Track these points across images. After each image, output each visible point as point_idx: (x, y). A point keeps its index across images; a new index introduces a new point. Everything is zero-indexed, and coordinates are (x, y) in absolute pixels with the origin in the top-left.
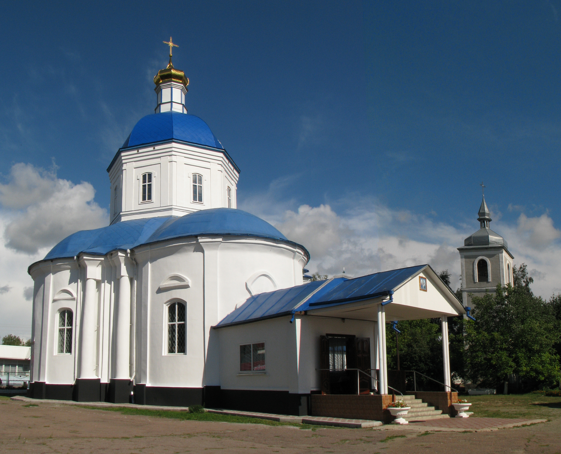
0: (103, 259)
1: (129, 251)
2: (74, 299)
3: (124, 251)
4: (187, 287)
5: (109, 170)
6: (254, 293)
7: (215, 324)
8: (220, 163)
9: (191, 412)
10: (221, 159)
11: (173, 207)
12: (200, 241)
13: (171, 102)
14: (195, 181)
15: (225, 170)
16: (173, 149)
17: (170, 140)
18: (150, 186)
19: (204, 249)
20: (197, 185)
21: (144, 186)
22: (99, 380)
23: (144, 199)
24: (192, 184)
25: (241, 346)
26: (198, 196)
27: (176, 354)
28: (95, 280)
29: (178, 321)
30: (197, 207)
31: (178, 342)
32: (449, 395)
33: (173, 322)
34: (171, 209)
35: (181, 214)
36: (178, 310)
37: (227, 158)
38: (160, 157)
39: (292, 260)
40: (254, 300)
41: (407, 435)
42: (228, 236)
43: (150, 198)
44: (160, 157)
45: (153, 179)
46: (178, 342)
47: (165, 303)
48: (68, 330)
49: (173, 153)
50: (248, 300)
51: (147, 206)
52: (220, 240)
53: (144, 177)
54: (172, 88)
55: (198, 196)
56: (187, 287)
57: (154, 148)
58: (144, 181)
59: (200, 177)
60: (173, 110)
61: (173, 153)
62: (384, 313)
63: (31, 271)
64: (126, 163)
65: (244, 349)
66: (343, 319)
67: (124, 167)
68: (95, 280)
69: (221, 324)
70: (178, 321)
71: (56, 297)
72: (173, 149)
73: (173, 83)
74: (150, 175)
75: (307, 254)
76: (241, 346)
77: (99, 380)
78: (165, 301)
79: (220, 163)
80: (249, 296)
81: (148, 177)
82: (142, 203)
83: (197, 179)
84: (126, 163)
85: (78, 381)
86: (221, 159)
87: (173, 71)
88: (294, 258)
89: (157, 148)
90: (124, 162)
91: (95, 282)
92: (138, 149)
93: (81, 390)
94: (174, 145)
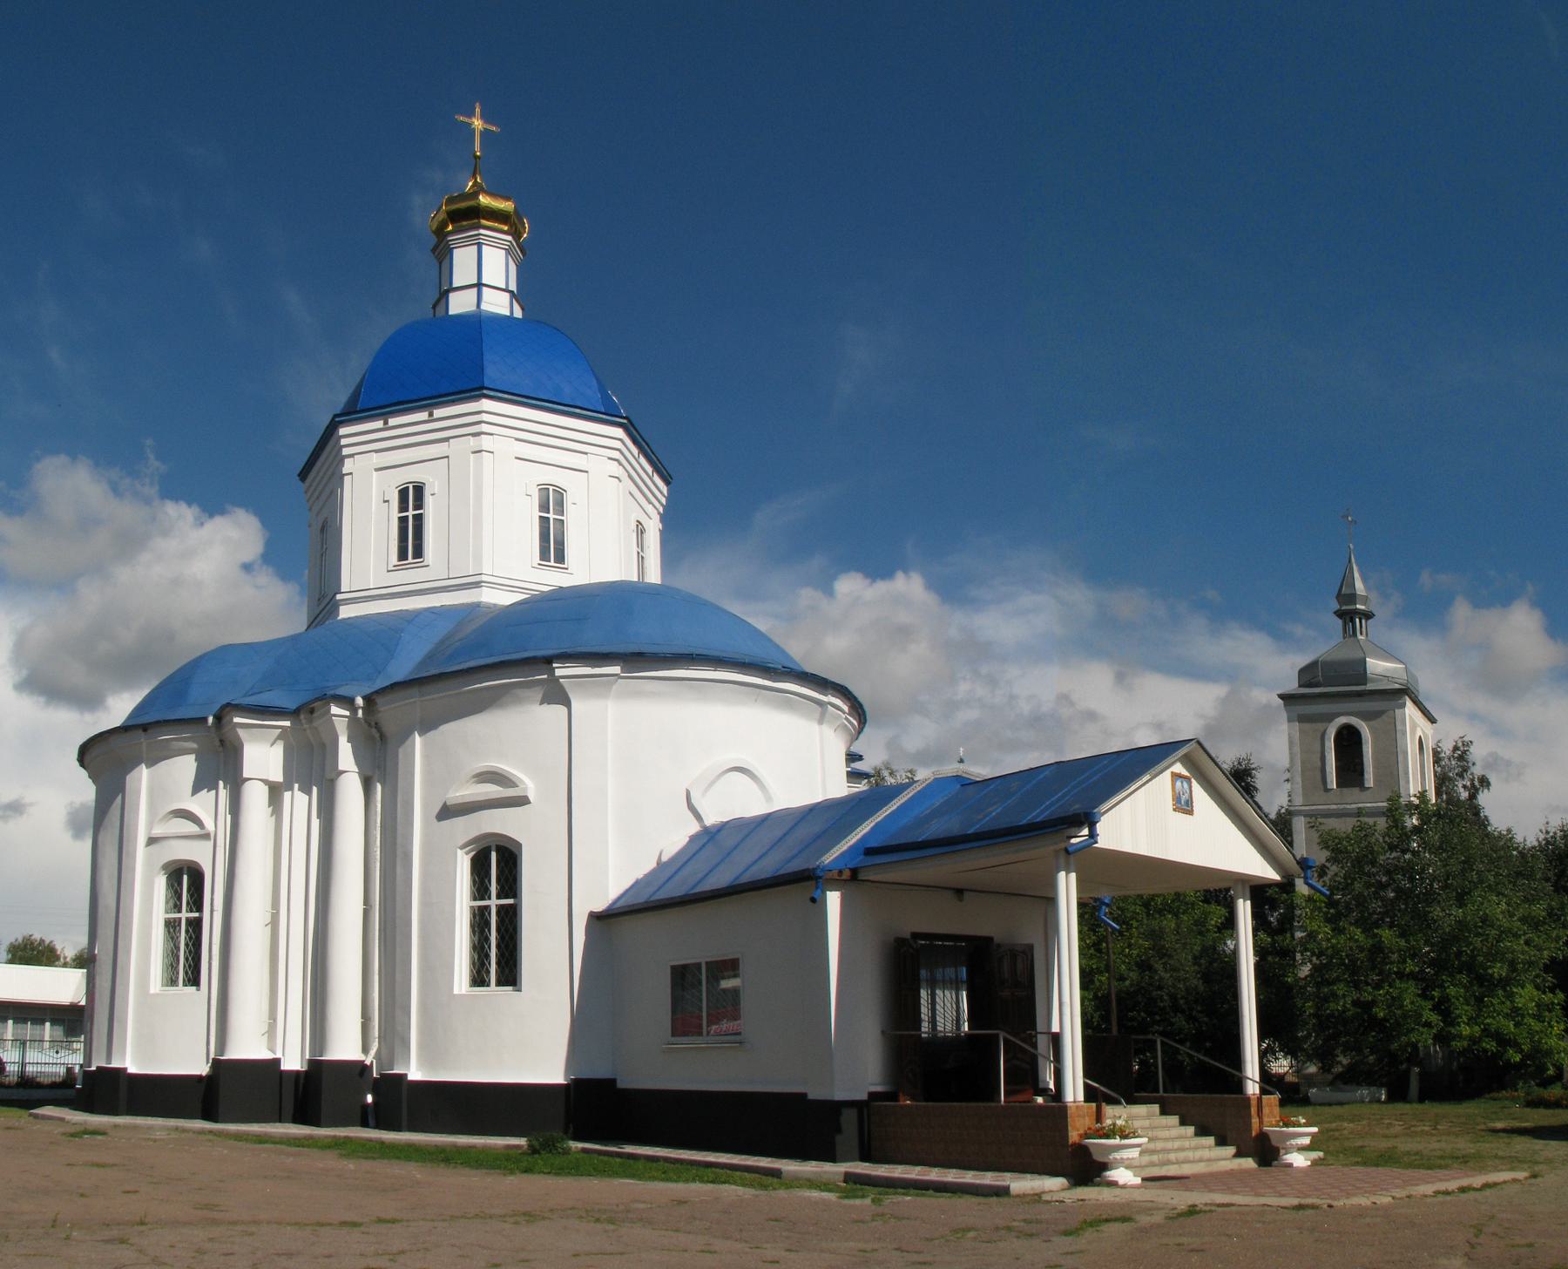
0: (288, 723)
1: (359, 701)
2: (206, 836)
3: (348, 702)
4: (522, 801)
5: (303, 475)
6: (711, 819)
7: (600, 906)
8: (616, 455)
9: (533, 1150)
10: (618, 444)
11: (484, 578)
12: (558, 672)
13: (479, 285)
14: (544, 507)
16: (485, 417)
17: (474, 390)
18: (419, 519)
20: (551, 516)
21: (403, 521)
22: (277, 1062)
23: (402, 555)
24: (537, 514)
25: (673, 968)
26: (552, 547)
27: (493, 991)
28: (265, 782)
29: (498, 897)
30: (551, 579)
31: (499, 956)
32: (1254, 1103)
33: (482, 899)
34: (477, 585)
35: (505, 599)
36: (498, 866)
38: (447, 440)
39: (815, 727)
40: (709, 837)
42: (637, 659)
43: (419, 553)
44: (447, 440)
45: (429, 501)
46: (499, 956)
48: (190, 922)
49: (485, 428)
50: (693, 839)
51: (412, 576)
52: (616, 669)
53: (403, 493)
54: (479, 245)
55: (552, 547)
56: (522, 801)
57: (431, 414)
58: (403, 506)
59: (560, 494)
61: (485, 428)
63: (87, 759)
64: (352, 456)
65: (682, 977)
66: (959, 892)
67: (348, 466)
68: (265, 782)
69: (619, 905)
70: (498, 897)
71: (158, 831)
72: (485, 417)
74: (419, 489)
75: (858, 709)
76: (673, 968)
77: (277, 1062)
79: (616, 455)
80: (695, 828)
81: (412, 496)
82: (397, 569)
83: (551, 501)
84: (352, 456)
85: (217, 1064)
86: (618, 444)
87: (484, 200)
88: (821, 722)
89: (438, 413)
90: (345, 451)
91: (266, 788)
93: (226, 1091)
94: (486, 404)
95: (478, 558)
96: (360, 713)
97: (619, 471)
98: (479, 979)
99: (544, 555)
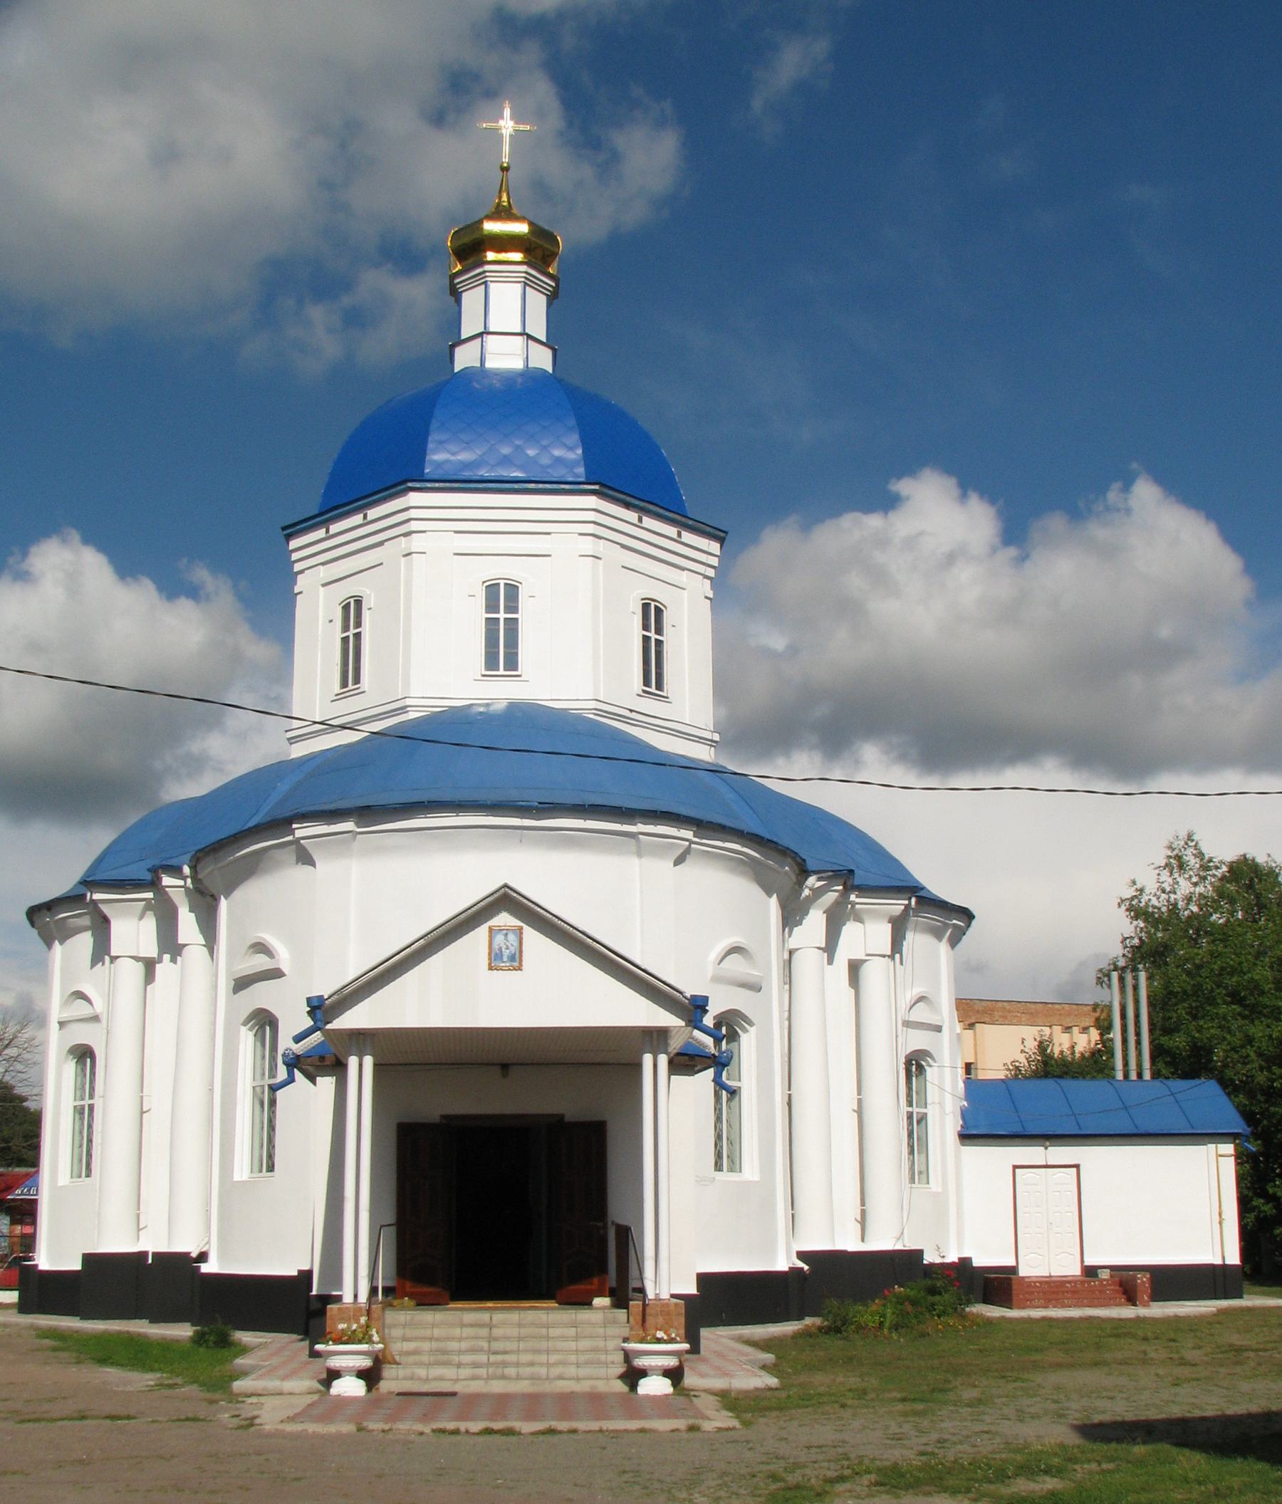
0: (150, 895)
1: (186, 870)
3: (175, 871)
4: (276, 974)
8: (590, 528)
9: (199, 1339)
11: (408, 702)
12: (299, 834)
14: (492, 606)
15: (323, 564)
16: (413, 513)
19: (315, 857)
20: (502, 615)
26: (502, 648)
28: (137, 959)
30: (499, 692)
37: (627, 506)
38: (381, 544)
39: (635, 861)
41: (1073, 1439)
42: (368, 813)
44: (381, 544)
45: (367, 616)
47: (245, 1024)
49: (414, 526)
52: (349, 826)
55: (502, 648)
56: (276, 974)
59: (512, 590)
60: (488, 365)
61: (414, 526)
62: (368, 1061)
64: (302, 572)
66: (505, 1067)
67: (302, 583)
68: (137, 959)
71: (65, 1015)
72: (413, 513)
73: (487, 268)
78: (242, 1020)
79: (590, 528)
81: (353, 611)
82: (339, 697)
83: (502, 598)
84: (302, 572)
87: (491, 227)
88: (640, 855)
89: (334, 528)
90: (297, 567)
91: (140, 965)
92: (326, 523)
94: (414, 498)
95: (407, 684)
96: (189, 881)
97: (588, 545)
98: (718, 1167)
99: (491, 662)
